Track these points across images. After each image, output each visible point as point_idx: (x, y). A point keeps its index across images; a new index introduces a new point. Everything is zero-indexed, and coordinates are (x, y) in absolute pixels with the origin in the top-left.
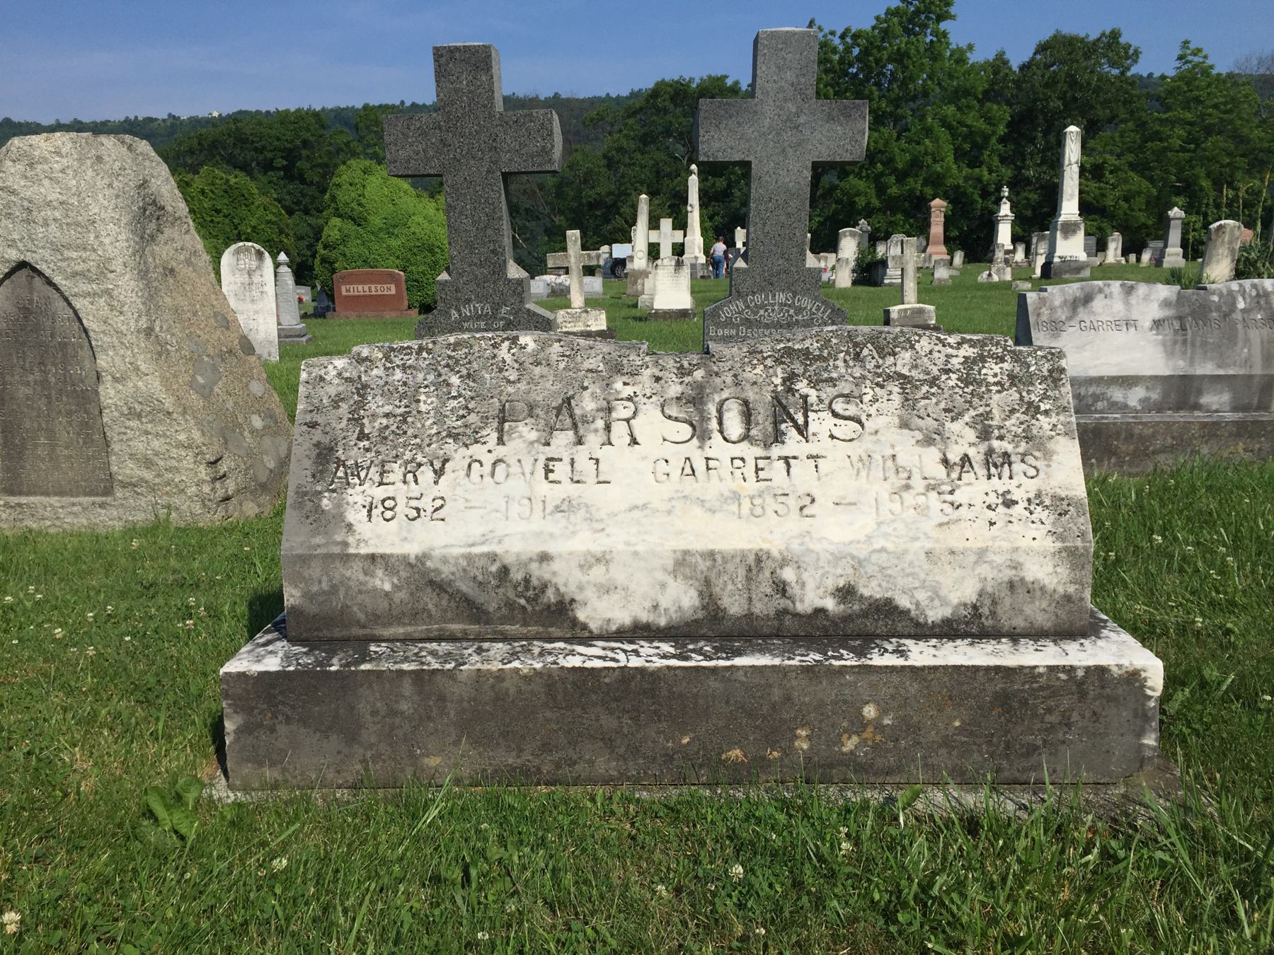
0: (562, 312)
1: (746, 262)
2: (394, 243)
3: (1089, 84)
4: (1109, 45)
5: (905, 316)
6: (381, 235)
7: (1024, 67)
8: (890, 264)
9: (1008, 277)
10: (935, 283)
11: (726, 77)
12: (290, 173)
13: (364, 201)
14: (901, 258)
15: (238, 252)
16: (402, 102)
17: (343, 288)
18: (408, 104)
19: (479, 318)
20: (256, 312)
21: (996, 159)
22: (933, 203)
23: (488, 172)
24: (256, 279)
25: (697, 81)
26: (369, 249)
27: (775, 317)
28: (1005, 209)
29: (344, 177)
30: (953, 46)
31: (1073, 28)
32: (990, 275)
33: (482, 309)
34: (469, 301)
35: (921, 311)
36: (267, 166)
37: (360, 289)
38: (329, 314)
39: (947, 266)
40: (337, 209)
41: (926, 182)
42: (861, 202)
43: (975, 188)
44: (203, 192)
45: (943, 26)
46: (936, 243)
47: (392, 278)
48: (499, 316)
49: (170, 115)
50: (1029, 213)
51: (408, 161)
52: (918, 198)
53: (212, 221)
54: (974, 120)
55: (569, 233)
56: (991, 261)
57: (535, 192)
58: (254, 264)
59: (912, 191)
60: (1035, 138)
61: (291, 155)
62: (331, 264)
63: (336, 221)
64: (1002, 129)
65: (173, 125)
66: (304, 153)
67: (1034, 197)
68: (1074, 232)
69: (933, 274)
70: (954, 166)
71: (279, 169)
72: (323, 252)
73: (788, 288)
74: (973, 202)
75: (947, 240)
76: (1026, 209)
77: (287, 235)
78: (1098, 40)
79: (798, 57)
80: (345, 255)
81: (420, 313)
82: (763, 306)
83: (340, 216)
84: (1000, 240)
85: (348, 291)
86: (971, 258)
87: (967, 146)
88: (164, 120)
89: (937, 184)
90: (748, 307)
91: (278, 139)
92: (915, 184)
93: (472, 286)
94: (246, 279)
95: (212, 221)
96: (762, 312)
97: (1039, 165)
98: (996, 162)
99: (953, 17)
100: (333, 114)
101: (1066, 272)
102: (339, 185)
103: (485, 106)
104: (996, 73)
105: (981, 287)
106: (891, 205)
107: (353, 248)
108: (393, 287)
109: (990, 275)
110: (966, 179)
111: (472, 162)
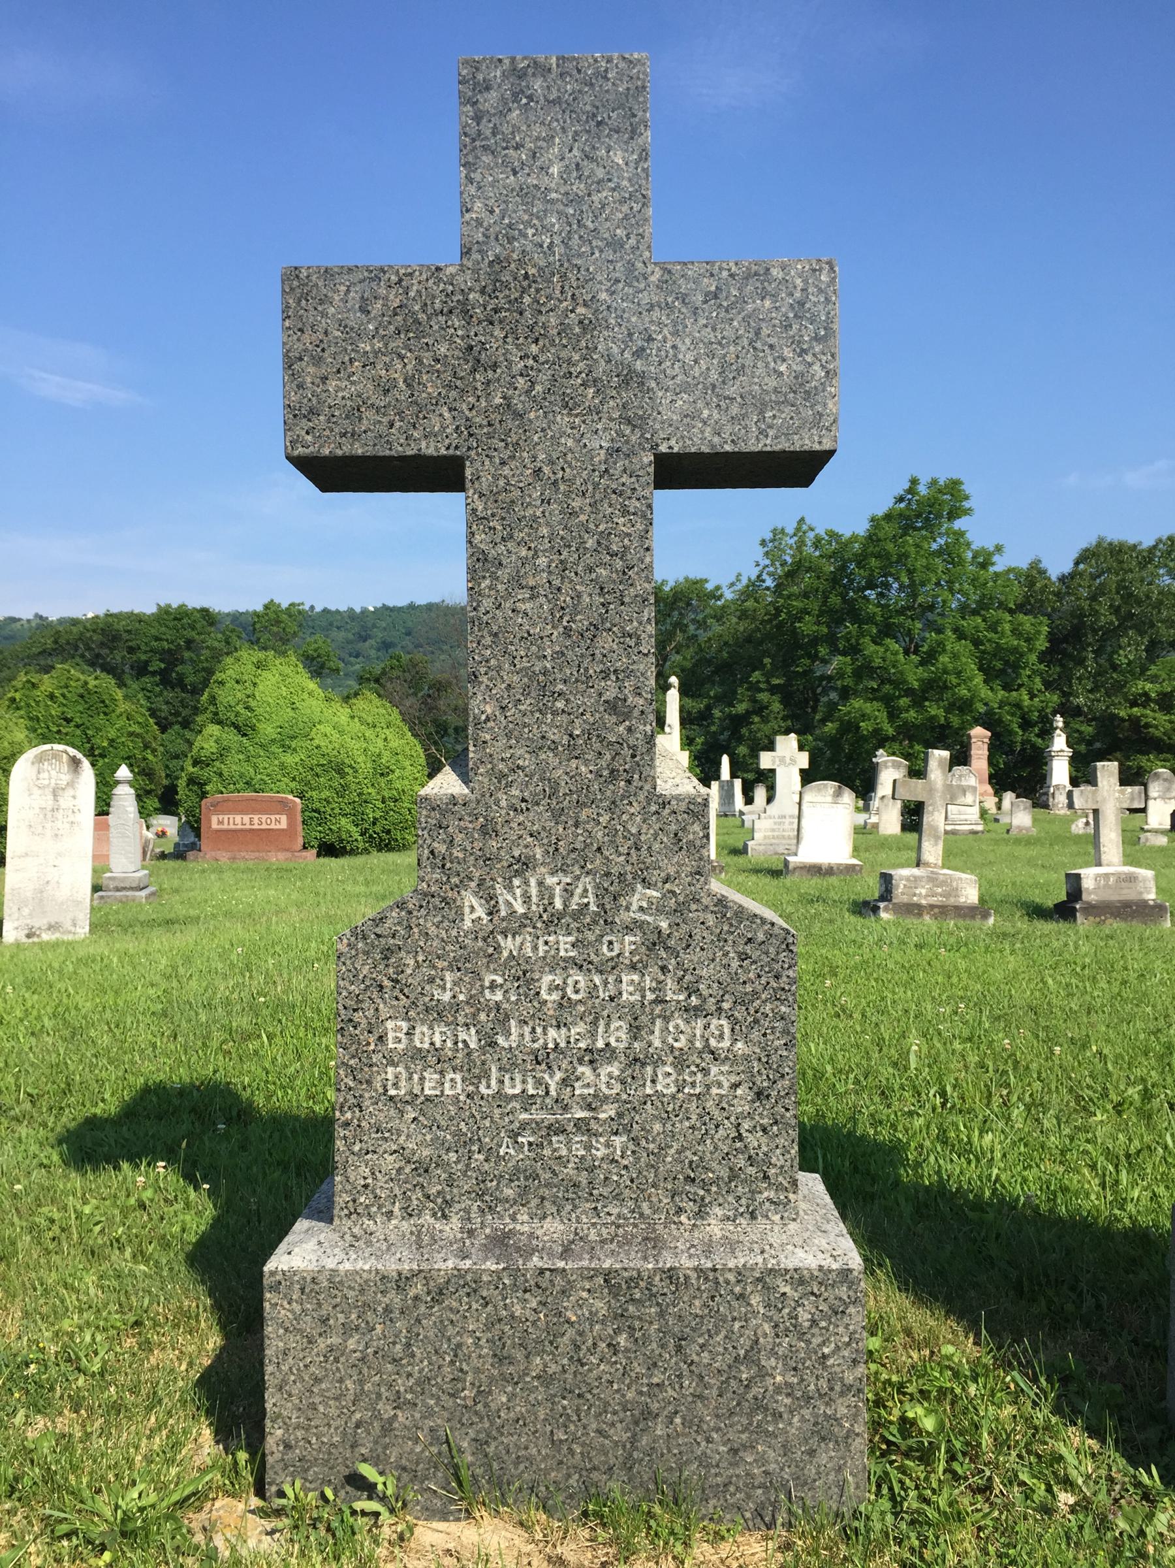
2: (290, 759)
3: (1148, 597)
5: (1107, 886)
6: (274, 749)
7: (1062, 579)
10: (1014, 832)
11: (706, 581)
12: (165, 679)
13: (253, 704)
15: (40, 759)
16: (312, 607)
17: (214, 819)
18: (318, 609)
19: (553, 921)
20: (59, 854)
21: (1038, 680)
23: (613, 452)
24: (65, 801)
25: (671, 584)
26: (255, 767)
28: (1060, 742)
31: (1117, 533)
33: (568, 892)
34: (524, 865)
35: (1131, 879)
36: (141, 670)
37: (239, 821)
38: (191, 855)
40: (216, 714)
43: (1013, 715)
45: (958, 524)
47: (283, 807)
48: (624, 917)
49: (37, 616)
51: (355, 413)
53: (59, 732)
58: (65, 778)
60: (1085, 659)
61: (171, 658)
62: (201, 785)
63: (213, 729)
64: (1042, 644)
65: (38, 627)
66: (187, 655)
67: (1088, 730)
71: (154, 673)
72: (191, 769)
74: (1011, 733)
77: (154, 751)
78: (1155, 547)
80: (221, 775)
81: (319, 855)
83: (220, 723)
84: (1055, 781)
85: (220, 822)
88: (29, 621)
91: (157, 639)
93: (538, 817)
94: (49, 802)
95: (59, 732)
97: (1091, 691)
98: (1038, 684)
102: (222, 683)
103: (616, 244)
107: (233, 766)
108: (284, 818)
111: (562, 420)
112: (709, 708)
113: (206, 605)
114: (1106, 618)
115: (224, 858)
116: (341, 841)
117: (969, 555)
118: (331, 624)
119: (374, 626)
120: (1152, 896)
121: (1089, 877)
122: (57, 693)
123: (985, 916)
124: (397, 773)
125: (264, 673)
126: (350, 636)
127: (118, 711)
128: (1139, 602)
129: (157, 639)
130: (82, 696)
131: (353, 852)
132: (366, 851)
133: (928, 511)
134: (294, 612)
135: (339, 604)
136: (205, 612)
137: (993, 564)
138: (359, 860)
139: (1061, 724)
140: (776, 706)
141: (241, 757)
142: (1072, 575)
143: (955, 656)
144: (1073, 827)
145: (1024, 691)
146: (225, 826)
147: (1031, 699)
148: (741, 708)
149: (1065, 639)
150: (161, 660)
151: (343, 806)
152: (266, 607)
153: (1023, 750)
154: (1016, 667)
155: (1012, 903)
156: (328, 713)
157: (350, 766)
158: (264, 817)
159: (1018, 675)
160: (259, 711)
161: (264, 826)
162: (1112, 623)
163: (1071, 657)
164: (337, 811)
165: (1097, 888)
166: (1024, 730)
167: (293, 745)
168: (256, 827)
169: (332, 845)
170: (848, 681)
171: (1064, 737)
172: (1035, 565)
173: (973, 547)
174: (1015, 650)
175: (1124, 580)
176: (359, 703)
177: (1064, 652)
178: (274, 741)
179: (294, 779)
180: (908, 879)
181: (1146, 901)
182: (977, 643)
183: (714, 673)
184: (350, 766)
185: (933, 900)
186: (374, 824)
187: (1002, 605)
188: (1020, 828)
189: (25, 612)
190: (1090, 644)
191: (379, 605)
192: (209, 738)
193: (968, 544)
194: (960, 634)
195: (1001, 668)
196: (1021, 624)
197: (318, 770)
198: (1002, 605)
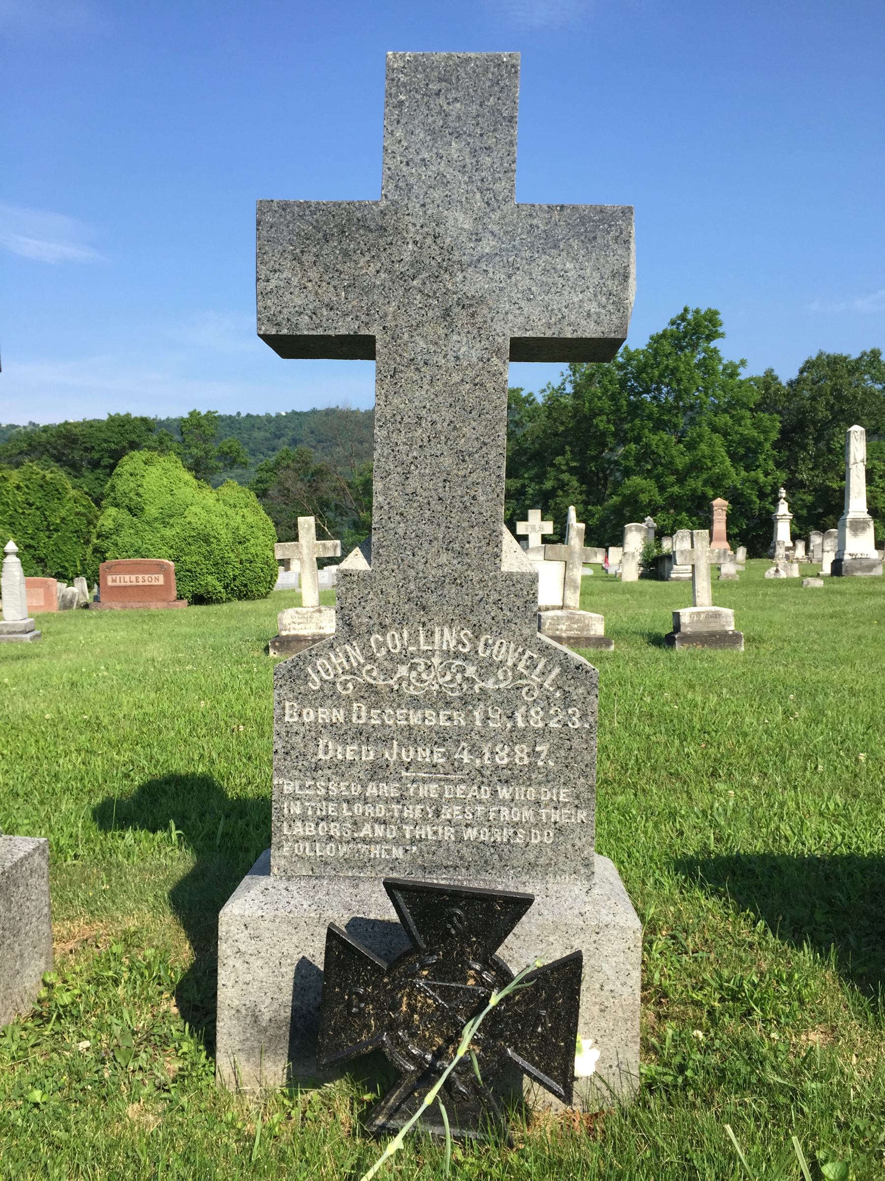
0: (291, 612)
1: (368, 557)
2: (168, 532)
3: (855, 397)
4: (871, 363)
5: (699, 621)
6: (156, 525)
7: (790, 384)
8: (679, 559)
9: (796, 574)
10: (722, 578)
11: (522, 389)
13: (141, 490)
14: (691, 553)
16: (239, 414)
17: (109, 578)
18: (243, 415)
21: (771, 463)
22: (715, 502)
27: (433, 681)
28: (783, 508)
29: (127, 467)
30: (725, 362)
31: (833, 349)
32: (777, 571)
35: (717, 615)
39: (735, 563)
40: (115, 499)
41: (705, 483)
42: (644, 498)
43: (752, 489)
44: (18, 487)
45: (712, 345)
46: (719, 539)
47: (160, 568)
49: (30, 423)
50: (804, 512)
52: (699, 498)
53: (23, 513)
54: (747, 430)
55: (301, 520)
56: (772, 557)
57: (344, 490)
59: (694, 490)
63: (112, 511)
64: (775, 436)
67: (809, 498)
68: (864, 529)
69: (719, 569)
70: (732, 470)
72: (95, 541)
73: (463, 617)
74: (751, 502)
75: (729, 537)
76: (801, 509)
78: (860, 358)
79: (474, 108)
80: (117, 545)
82: (405, 658)
86: (752, 554)
87: (741, 451)
88: (25, 427)
89: (717, 484)
90: (371, 658)
91: (106, 441)
92: (695, 483)
95: (23, 513)
96: (403, 670)
97: (812, 469)
98: (771, 465)
99: (722, 335)
100: (176, 424)
101: (857, 570)
104: (767, 389)
105: (769, 583)
106: (674, 503)
107: (126, 538)
109: (777, 571)
110: (745, 481)
112: (524, 486)
113: (144, 416)
114: (823, 413)
115: (117, 607)
116: (209, 593)
117: (721, 368)
118: (253, 426)
119: (286, 427)
120: (732, 628)
121: (686, 615)
122: (21, 484)
123: (608, 644)
124: (252, 541)
125: (150, 468)
126: (268, 435)
127: (68, 496)
128: (848, 401)
129: (106, 441)
130: (41, 486)
131: (218, 601)
132: (229, 600)
133: (695, 330)
134: (211, 418)
135: (259, 410)
136: (144, 420)
137: (738, 375)
138: (225, 607)
139: (784, 495)
140: (575, 484)
141: (132, 531)
142: (798, 381)
143: (711, 445)
144: (766, 573)
145: (760, 471)
146: (118, 584)
147: (766, 476)
148: (548, 485)
149: (794, 430)
150: (109, 457)
151: (209, 567)
152: (191, 414)
153: (760, 514)
154: (755, 452)
155: (642, 634)
156: (199, 497)
157: (215, 537)
158: (146, 576)
159: (757, 459)
160: (146, 496)
161: (147, 583)
162: (827, 417)
163: (798, 444)
164: (205, 571)
165: (692, 622)
166: (761, 500)
167: (171, 521)
168: (141, 583)
169: (202, 596)
170: (631, 463)
171: (786, 504)
172: (769, 373)
173: (725, 362)
174: (753, 440)
175: (835, 384)
176: (224, 490)
177: (791, 440)
178: (156, 519)
179: (172, 547)
180: (552, 619)
181: (727, 632)
182: (725, 435)
183: (529, 460)
184: (215, 537)
185: (571, 634)
186: (234, 579)
187: (744, 406)
188: (727, 575)
189: (22, 421)
190: (811, 433)
191: (289, 411)
192: (110, 516)
193: (720, 360)
194: (715, 429)
195: (745, 454)
196: (761, 420)
197: (190, 540)
198: (744, 406)
